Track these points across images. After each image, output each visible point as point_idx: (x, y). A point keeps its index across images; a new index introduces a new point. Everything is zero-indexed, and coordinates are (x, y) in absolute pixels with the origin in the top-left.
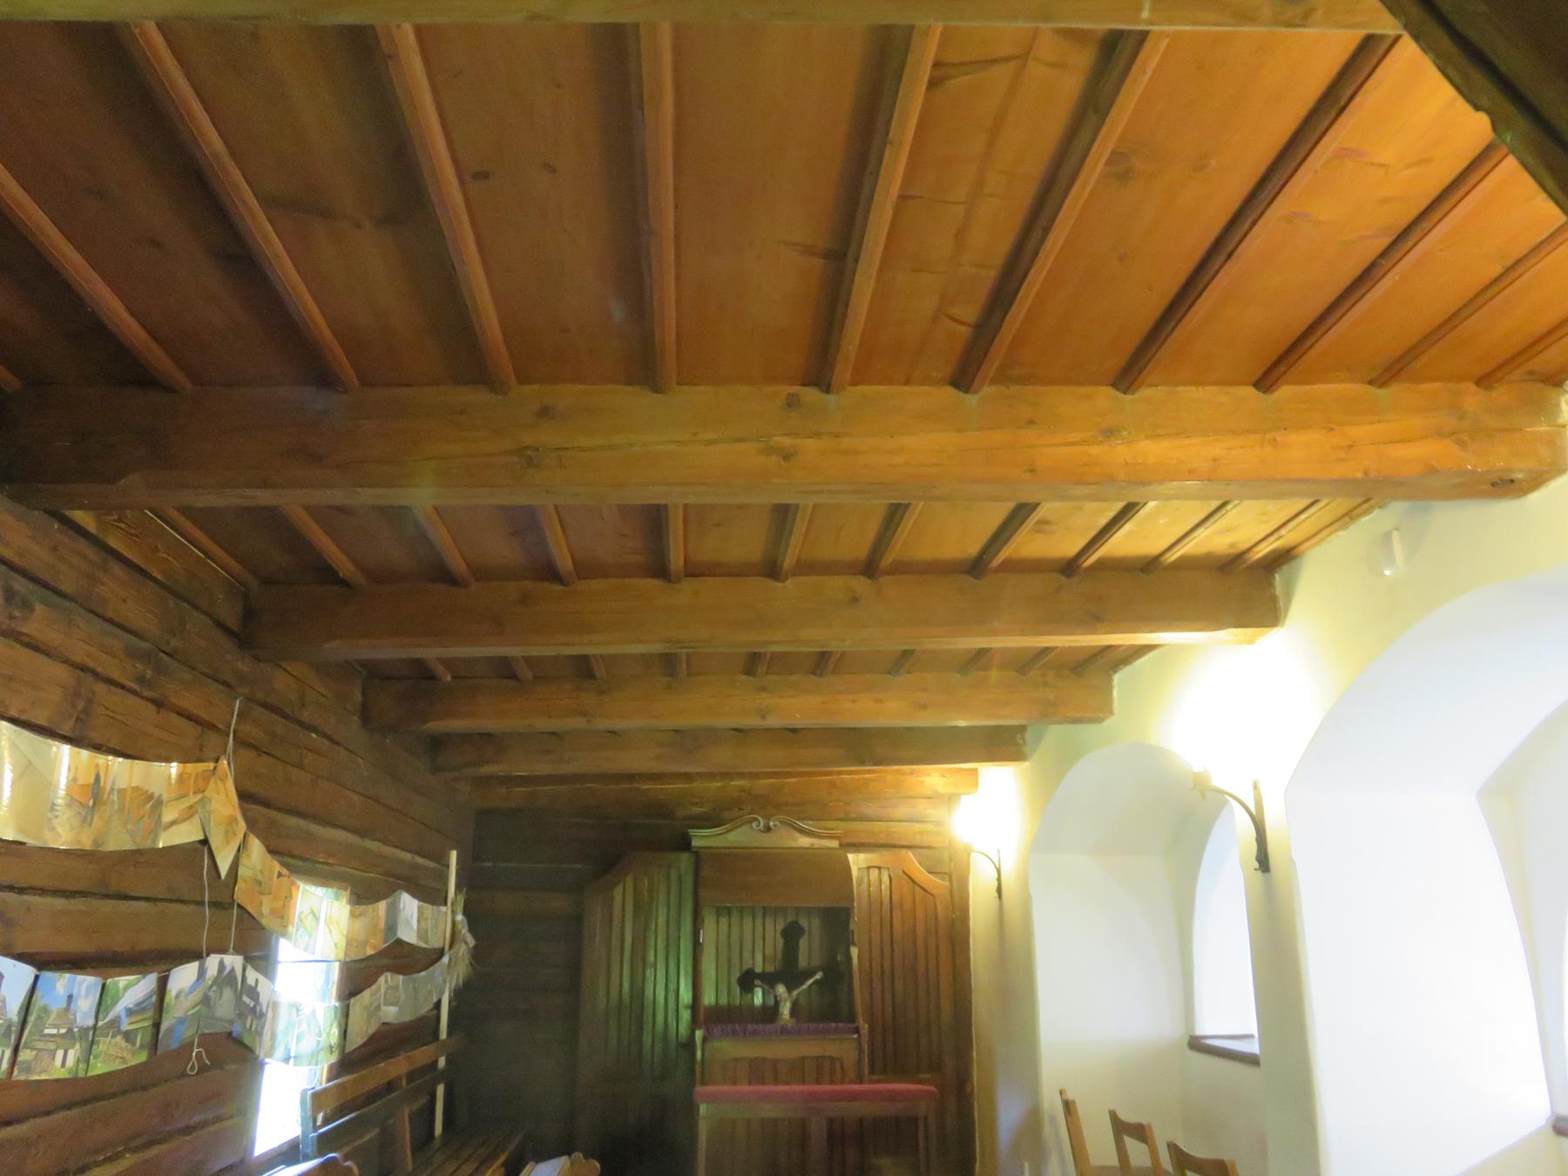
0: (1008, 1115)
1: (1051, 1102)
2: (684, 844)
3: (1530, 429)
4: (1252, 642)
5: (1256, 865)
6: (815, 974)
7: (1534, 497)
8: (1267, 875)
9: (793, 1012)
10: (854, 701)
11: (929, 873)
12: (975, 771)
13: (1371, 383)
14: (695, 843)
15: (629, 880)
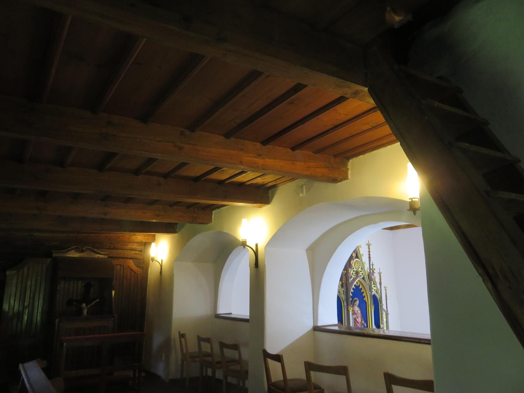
0: (157, 340)
1: (175, 334)
2: (49, 255)
3: (342, 169)
4: (260, 207)
5: (254, 266)
6: (97, 300)
7: (339, 184)
8: (257, 269)
9: (87, 312)
10: (136, 212)
11: (137, 267)
12: (155, 235)
13: (314, 152)
14: (54, 255)
15: (26, 268)
